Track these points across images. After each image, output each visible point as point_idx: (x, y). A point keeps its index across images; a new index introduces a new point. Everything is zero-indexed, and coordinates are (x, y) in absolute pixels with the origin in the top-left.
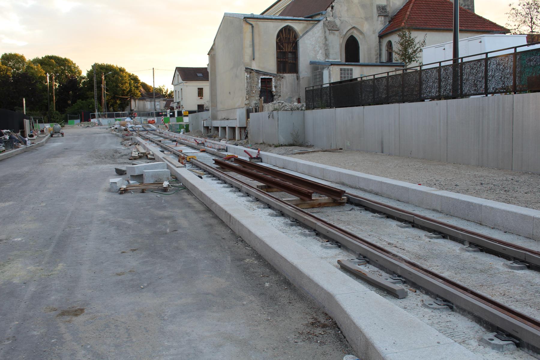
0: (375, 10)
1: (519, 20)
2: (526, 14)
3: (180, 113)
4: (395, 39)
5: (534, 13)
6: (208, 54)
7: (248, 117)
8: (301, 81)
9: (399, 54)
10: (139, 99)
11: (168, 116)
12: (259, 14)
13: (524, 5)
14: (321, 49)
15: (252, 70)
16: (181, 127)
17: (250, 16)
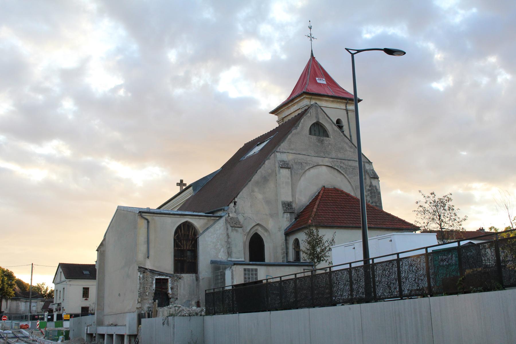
0: (280, 207)
1: (427, 217)
2: (434, 211)
3: (60, 317)
4: (302, 237)
5: (441, 211)
6: (97, 250)
7: (139, 323)
8: (201, 283)
9: (306, 253)
10: (12, 299)
11: (46, 320)
12: (155, 208)
13: (431, 203)
14: (223, 247)
15: (146, 269)
16: (60, 333)
17: (145, 210)
